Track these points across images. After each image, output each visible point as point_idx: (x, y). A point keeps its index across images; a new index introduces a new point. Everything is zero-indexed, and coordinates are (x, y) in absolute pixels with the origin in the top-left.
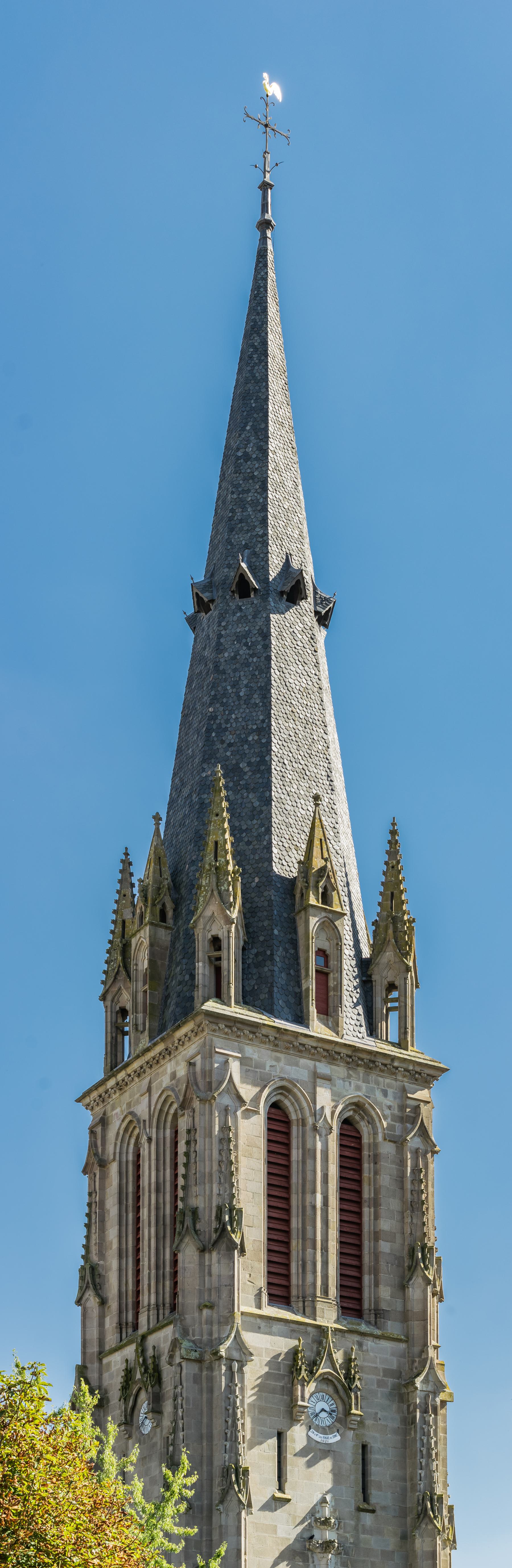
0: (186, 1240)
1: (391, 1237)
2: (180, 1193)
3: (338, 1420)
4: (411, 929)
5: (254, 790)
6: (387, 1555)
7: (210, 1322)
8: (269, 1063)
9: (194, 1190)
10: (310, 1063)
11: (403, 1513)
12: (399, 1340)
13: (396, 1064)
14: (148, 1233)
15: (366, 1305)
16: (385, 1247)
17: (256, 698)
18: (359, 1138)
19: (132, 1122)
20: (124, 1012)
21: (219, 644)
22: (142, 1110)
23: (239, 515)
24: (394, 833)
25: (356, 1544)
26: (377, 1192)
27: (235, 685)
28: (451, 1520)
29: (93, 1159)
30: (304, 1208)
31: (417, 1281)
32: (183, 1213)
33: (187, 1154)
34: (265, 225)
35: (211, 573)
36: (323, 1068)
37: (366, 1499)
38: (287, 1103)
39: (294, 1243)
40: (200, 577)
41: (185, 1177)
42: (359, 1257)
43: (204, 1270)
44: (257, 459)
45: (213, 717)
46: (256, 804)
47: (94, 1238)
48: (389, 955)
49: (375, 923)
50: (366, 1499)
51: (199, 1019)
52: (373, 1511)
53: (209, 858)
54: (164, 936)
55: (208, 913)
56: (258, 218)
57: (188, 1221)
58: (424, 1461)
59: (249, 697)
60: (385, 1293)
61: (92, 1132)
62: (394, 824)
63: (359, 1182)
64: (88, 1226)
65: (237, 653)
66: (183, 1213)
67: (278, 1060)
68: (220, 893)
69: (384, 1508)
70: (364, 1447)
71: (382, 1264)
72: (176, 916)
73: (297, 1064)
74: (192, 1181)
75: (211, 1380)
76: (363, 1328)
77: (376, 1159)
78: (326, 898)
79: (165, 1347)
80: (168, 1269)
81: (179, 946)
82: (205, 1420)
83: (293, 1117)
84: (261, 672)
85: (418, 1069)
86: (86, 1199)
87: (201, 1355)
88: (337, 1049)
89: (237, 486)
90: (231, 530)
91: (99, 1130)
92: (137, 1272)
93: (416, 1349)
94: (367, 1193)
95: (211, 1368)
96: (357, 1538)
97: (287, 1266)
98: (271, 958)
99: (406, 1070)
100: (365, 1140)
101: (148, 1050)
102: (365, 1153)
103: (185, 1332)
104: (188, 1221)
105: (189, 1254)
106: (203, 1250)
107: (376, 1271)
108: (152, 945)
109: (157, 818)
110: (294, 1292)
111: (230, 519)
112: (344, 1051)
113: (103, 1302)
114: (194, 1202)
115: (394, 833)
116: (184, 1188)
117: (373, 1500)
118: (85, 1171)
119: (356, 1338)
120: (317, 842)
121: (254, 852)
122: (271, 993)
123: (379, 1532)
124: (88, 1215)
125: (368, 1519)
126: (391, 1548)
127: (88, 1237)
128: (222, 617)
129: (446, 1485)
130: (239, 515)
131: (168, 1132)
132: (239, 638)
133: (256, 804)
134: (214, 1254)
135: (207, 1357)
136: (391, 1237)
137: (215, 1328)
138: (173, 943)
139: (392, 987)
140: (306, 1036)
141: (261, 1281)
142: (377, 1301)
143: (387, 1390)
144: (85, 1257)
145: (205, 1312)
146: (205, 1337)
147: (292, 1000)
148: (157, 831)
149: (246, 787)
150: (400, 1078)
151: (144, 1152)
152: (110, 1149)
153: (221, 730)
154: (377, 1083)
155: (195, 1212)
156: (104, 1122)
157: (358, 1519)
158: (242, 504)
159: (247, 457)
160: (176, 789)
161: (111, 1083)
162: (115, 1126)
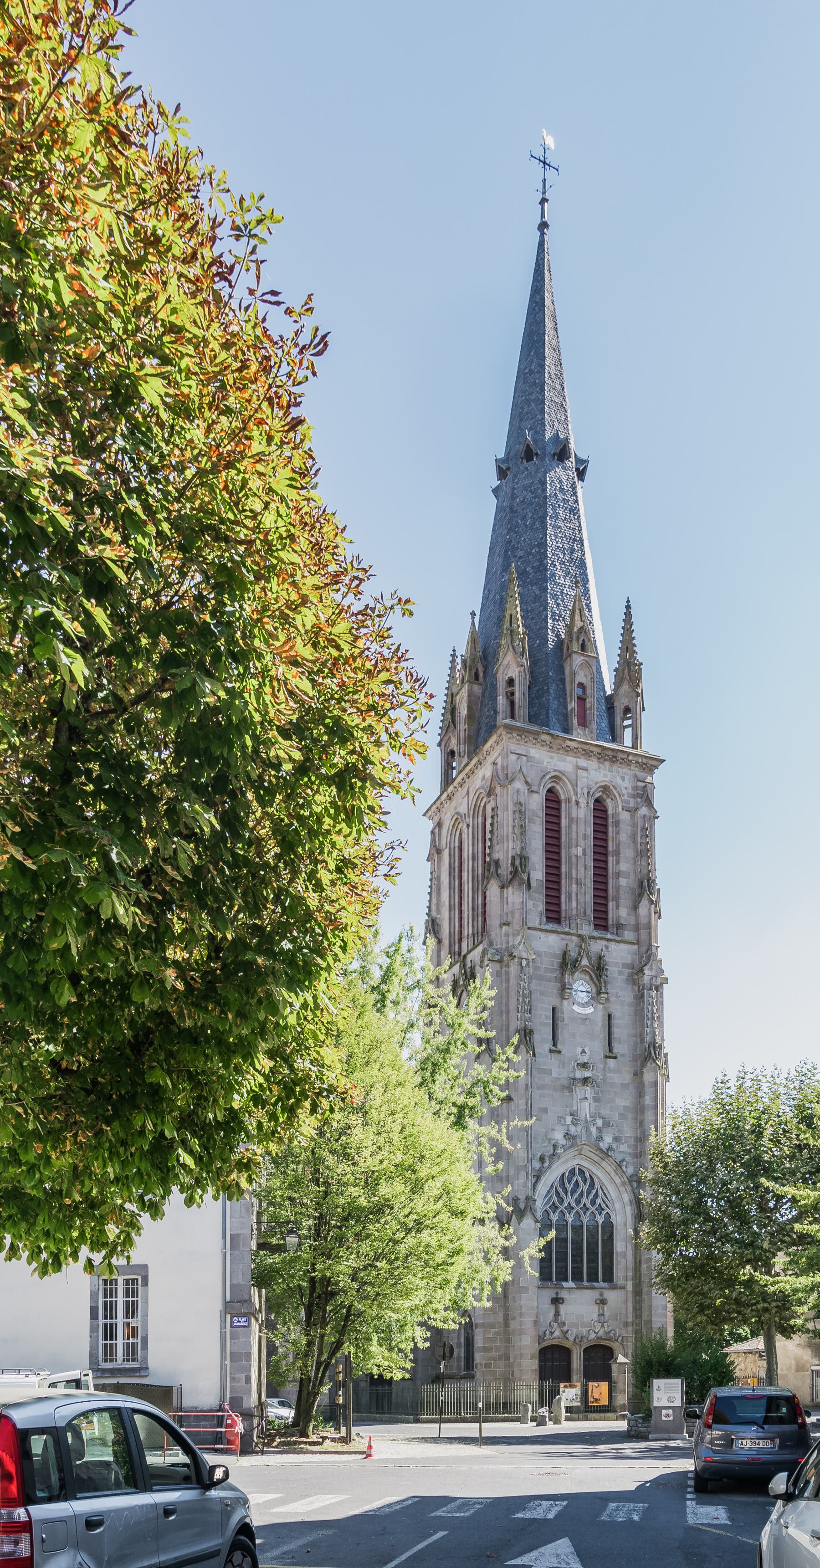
0: (492, 881)
1: (627, 875)
2: (488, 851)
3: (592, 998)
4: (640, 669)
5: (536, 584)
6: (624, 1086)
7: (507, 935)
8: (546, 760)
9: (497, 847)
10: (573, 760)
11: (635, 1058)
12: (633, 943)
13: (630, 758)
14: (467, 887)
15: (611, 922)
16: (623, 882)
17: (537, 525)
18: (606, 811)
19: (458, 818)
20: (452, 753)
21: (513, 494)
22: (463, 809)
23: (526, 410)
24: (628, 607)
25: (604, 1080)
26: (618, 845)
27: (524, 518)
28: (666, 1062)
29: (434, 850)
30: (570, 858)
31: (644, 903)
32: (489, 864)
33: (492, 825)
34: (543, 226)
35: (508, 453)
36: (582, 762)
37: (610, 1050)
38: (558, 787)
39: (563, 881)
40: (501, 455)
41: (490, 840)
42: (606, 891)
43: (503, 900)
44: (538, 372)
45: (509, 542)
46: (538, 592)
47: (434, 901)
48: (625, 687)
49: (616, 670)
50: (610, 1050)
51: (499, 732)
52: (615, 1058)
53: (507, 625)
54: (477, 689)
55: (505, 662)
56: (539, 221)
57: (493, 869)
58: (649, 1022)
59: (533, 524)
60: (623, 912)
61: (433, 832)
62: (628, 601)
63: (606, 840)
64: (430, 894)
65: (525, 498)
66: (489, 864)
67: (552, 758)
68: (513, 648)
69: (623, 1055)
70: (609, 1016)
71: (622, 893)
72: (485, 677)
73: (565, 761)
74: (495, 842)
75: (508, 974)
76: (609, 936)
77: (617, 824)
78: (583, 647)
79: (477, 960)
80: (480, 910)
81: (487, 694)
82: (504, 1001)
83: (562, 797)
84: (541, 507)
85: (645, 761)
86: (429, 877)
87: (502, 957)
88: (592, 749)
89: (524, 392)
90: (521, 420)
91: (437, 831)
92: (461, 919)
93: (644, 949)
94: (611, 847)
95: (508, 966)
96: (605, 1075)
97: (559, 898)
98: (548, 691)
99: (637, 762)
100: (610, 812)
101: (467, 765)
102: (610, 820)
103: (491, 944)
104: (493, 869)
105: (493, 889)
106: (502, 887)
107: (617, 899)
108: (469, 696)
109: (473, 614)
110: (563, 915)
111: (520, 413)
112: (596, 750)
113: (440, 942)
114: (496, 856)
115: (628, 607)
116: (490, 847)
117: (615, 1050)
118: (428, 860)
119: (604, 943)
120: (577, 611)
121: (536, 623)
122: (547, 714)
123: (618, 1071)
124: (430, 887)
125: (611, 1063)
126: (627, 1082)
127: (430, 901)
128: (515, 476)
129: (663, 1040)
130: (526, 410)
131: (480, 819)
132: (525, 488)
133: (538, 592)
134: (510, 889)
135: (505, 958)
136: (627, 875)
137: (511, 939)
138: (483, 693)
139: (627, 710)
140: (571, 740)
141: (541, 907)
142: (618, 918)
143: (624, 977)
144: (428, 914)
145: (504, 928)
146: (504, 946)
147: (561, 718)
148: (473, 623)
149: (532, 583)
150: (633, 767)
151: (465, 836)
152: (444, 841)
153: (514, 549)
154: (618, 772)
155: (497, 863)
156: (439, 825)
157: (606, 1063)
158: (528, 402)
159: (531, 372)
160: (485, 598)
161: (445, 795)
162: (447, 824)
